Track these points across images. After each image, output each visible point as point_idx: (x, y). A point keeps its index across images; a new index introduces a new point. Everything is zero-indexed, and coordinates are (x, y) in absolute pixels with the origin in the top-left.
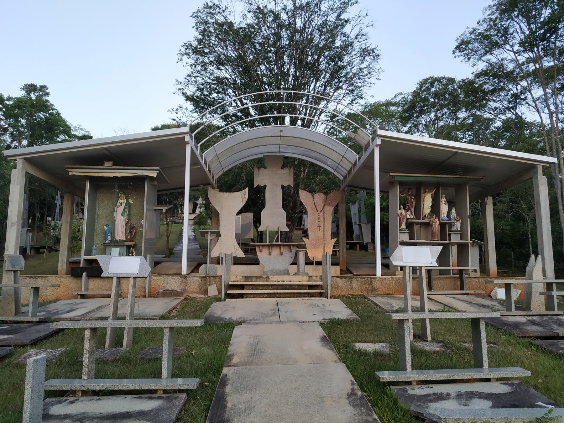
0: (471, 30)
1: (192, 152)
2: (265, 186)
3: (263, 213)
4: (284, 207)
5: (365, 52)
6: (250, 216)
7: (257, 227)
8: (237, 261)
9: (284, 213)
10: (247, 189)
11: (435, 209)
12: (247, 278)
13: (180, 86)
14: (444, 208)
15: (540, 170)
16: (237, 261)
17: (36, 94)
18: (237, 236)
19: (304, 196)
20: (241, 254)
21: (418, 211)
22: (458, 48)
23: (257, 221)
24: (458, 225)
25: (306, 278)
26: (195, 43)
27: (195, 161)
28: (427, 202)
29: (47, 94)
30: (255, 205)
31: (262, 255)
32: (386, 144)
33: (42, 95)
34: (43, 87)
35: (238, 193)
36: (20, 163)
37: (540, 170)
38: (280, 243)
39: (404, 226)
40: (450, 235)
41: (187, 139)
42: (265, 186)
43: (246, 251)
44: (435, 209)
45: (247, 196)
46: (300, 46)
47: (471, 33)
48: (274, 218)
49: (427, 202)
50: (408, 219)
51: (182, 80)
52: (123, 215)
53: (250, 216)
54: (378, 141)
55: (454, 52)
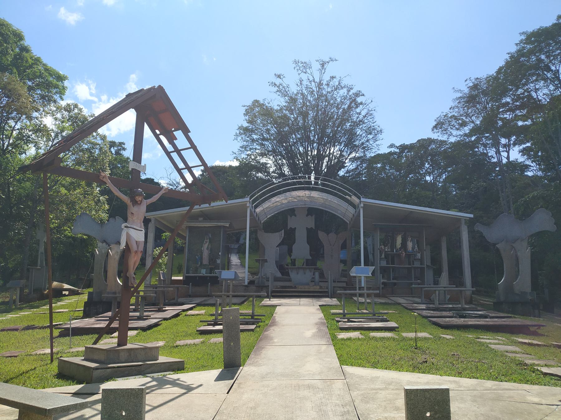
0: (444, 114)
1: (250, 210)
2: (295, 228)
3: (294, 247)
4: (308, 243)
5: (369, 131)
6: (285, 248)
7: (290, 256)
8: (276, 279)
9: (308, 247)
10: (283, 231)
11: (404, 244)
12: (283, 287)
13: (235, 155)
14: (410, 245)
15: (463, 222)
16: (276, 279)
17: (115, 148)
18: (276, 262)
19: (322, 235)
20: (279, 275)
21: (393, 245)
22: (435, 127)
23: (290, 251)
24: (419, 256)
25: (318, 287)
26: (246, 124)
27: (251, 215)
28: (399, 240)
29: (124, 149)
30: (289, 239)
31: (293, 275)
32: (366, 207)
33: (120, 150)
34: (121, 144)
35: (277, 233)
36: (153, 222)
37: (463, 222)
38: (305, 266)
39: (383, 256)
40: (413, 262)
41: (248, 205)
42: (295, 228)
43: (283, 274)
44: (404, 244)
45: (283, 235)
46: (322, 121)
47: (445, 116)
48: (301, 250)
49: (399, 240)
50: (386, 252)
51: (236, 151)
52: (207, 249)
53: (285, 248)
54: (362, 205)
55: (433, 130)
